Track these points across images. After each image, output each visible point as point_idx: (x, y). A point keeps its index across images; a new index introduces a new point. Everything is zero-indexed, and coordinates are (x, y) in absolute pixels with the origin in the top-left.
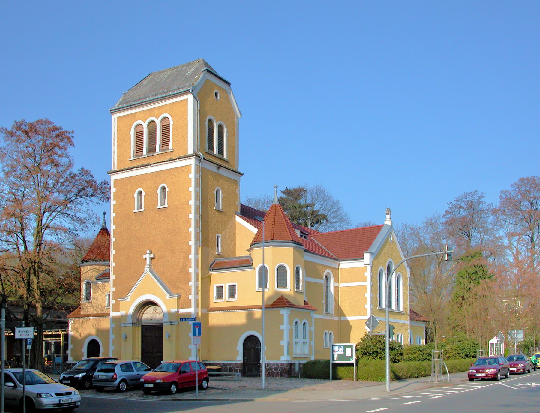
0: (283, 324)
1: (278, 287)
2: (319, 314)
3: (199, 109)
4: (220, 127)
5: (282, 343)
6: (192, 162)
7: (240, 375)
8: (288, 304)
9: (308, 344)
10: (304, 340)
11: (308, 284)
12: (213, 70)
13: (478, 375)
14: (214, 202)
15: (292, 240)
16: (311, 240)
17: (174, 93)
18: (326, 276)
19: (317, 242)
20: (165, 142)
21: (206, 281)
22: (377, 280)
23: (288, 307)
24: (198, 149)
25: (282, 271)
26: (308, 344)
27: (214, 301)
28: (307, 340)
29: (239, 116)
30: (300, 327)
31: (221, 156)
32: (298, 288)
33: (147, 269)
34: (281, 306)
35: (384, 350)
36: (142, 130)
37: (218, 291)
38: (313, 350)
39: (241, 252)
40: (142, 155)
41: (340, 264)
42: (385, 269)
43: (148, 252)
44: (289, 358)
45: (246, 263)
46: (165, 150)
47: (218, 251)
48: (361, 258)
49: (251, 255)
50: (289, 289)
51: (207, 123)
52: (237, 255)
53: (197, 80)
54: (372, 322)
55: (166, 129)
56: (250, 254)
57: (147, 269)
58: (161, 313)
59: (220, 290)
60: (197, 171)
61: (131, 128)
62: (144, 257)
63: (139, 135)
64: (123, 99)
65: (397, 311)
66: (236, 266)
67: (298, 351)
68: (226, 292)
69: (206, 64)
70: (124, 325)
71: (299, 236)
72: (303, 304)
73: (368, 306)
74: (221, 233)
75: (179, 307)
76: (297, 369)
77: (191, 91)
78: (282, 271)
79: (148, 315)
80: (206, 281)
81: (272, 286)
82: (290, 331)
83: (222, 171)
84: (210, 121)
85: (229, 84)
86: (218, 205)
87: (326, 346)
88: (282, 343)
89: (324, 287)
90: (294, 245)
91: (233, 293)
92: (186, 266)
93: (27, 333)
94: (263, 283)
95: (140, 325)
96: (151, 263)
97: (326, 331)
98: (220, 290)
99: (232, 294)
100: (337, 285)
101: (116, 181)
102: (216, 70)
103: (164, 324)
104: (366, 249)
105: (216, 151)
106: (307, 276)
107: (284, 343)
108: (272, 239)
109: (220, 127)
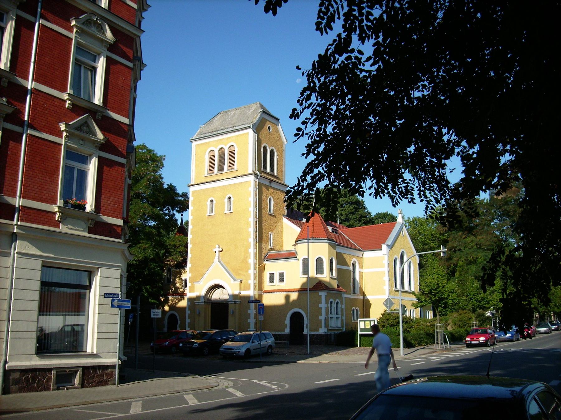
0: (321, 303)
1: (317, 274)
2: (348, 294)
3: (257, 139)
4: (272, 152)
5: (320, 318)
6: (252, 178)
7: (289, 343)
8: (325, 288)
9: (340, 319)
10: (338, 316)
11: (339, 270)
12: (267, 110)
13: (473, 342)
14: (268, 208)
15: (327, 238)
16: (340, 234)
17: (238, 128)
18: (353, 264)
19: (345, 236)
20: (232, 164)
21: (261, 270)
22: (392, 266)
23: (325, 290)
24: (256, 169)
25: (319, 261)
26: (340, 319)
27: (267, 285)
28: (339, 316)
29: (286, 142)
30: (334, 305)
31: (272, 173)
32: (332, 275)
33: (216, 260)
34: (319, 289)
35: (398, 323)
36: (214, 154)
37: (270, 277)
38: (344, 323)
39: (288, 246)
40: (213, 173)
41: (363, 254)
42: (399, 257)
43: (217, 246)
44: (326, 330)
45: (292, 256)
46: (232, 169)
47: (270, 246)
48: (380, 249)
49: (296, 249)
50: (325, 277)
51: (262, 150)
52: (285, 249)
53: (255, 118)
54: (388, 303)
55: (232, 154)
56: (295, 249)
57: (216, 260)
58: (226, 294)
59: (272, 276)
60: (255, 186)
61: (205, 153)
62: (214, 250)
63: (212, 158)
64: (200, 131)
65: (409, 291)
66: (284, 258)
67: (7, 182)
68: (277, 278)
69: (262, 107)
70: (198, 303)
71: (331, 231)
72: (336, 287)
73: (386, 288)
74: (272, 232)
75: (240, 289)
76: (333, 338)
77: (251, 127)
78: (319, 261)
79: (217, 295)
80: (261, 270)
81: (312, 272)
82: (327, 309)
83: (273, 185)
84: (265, 148)
85: (278, 120)
86: (270, 210)
87: (353, 320)
88: (320, 318)
89: (352, 273)
90: (328, 241)
91: (282, 278)
92: (247, 257)
93: (157, 314)
94: (306, 270)
95: (210, 303)
96: (219, 255)
97: (354, 308)
98: (272, 276)
99: (282, 279)
100: (361, 270)
101: (194, 192)
102: (269, 111)
103: (229, 303)
104: (384, 242)
105: (269, 170)
106: (338, 265)
107: (322, 318)
108: (312, 237)
109: (272, 152)
